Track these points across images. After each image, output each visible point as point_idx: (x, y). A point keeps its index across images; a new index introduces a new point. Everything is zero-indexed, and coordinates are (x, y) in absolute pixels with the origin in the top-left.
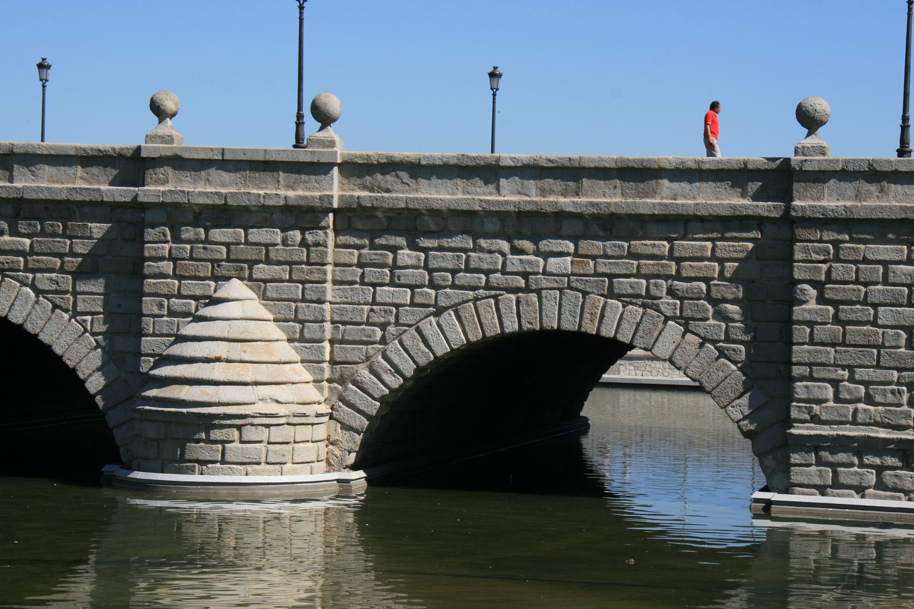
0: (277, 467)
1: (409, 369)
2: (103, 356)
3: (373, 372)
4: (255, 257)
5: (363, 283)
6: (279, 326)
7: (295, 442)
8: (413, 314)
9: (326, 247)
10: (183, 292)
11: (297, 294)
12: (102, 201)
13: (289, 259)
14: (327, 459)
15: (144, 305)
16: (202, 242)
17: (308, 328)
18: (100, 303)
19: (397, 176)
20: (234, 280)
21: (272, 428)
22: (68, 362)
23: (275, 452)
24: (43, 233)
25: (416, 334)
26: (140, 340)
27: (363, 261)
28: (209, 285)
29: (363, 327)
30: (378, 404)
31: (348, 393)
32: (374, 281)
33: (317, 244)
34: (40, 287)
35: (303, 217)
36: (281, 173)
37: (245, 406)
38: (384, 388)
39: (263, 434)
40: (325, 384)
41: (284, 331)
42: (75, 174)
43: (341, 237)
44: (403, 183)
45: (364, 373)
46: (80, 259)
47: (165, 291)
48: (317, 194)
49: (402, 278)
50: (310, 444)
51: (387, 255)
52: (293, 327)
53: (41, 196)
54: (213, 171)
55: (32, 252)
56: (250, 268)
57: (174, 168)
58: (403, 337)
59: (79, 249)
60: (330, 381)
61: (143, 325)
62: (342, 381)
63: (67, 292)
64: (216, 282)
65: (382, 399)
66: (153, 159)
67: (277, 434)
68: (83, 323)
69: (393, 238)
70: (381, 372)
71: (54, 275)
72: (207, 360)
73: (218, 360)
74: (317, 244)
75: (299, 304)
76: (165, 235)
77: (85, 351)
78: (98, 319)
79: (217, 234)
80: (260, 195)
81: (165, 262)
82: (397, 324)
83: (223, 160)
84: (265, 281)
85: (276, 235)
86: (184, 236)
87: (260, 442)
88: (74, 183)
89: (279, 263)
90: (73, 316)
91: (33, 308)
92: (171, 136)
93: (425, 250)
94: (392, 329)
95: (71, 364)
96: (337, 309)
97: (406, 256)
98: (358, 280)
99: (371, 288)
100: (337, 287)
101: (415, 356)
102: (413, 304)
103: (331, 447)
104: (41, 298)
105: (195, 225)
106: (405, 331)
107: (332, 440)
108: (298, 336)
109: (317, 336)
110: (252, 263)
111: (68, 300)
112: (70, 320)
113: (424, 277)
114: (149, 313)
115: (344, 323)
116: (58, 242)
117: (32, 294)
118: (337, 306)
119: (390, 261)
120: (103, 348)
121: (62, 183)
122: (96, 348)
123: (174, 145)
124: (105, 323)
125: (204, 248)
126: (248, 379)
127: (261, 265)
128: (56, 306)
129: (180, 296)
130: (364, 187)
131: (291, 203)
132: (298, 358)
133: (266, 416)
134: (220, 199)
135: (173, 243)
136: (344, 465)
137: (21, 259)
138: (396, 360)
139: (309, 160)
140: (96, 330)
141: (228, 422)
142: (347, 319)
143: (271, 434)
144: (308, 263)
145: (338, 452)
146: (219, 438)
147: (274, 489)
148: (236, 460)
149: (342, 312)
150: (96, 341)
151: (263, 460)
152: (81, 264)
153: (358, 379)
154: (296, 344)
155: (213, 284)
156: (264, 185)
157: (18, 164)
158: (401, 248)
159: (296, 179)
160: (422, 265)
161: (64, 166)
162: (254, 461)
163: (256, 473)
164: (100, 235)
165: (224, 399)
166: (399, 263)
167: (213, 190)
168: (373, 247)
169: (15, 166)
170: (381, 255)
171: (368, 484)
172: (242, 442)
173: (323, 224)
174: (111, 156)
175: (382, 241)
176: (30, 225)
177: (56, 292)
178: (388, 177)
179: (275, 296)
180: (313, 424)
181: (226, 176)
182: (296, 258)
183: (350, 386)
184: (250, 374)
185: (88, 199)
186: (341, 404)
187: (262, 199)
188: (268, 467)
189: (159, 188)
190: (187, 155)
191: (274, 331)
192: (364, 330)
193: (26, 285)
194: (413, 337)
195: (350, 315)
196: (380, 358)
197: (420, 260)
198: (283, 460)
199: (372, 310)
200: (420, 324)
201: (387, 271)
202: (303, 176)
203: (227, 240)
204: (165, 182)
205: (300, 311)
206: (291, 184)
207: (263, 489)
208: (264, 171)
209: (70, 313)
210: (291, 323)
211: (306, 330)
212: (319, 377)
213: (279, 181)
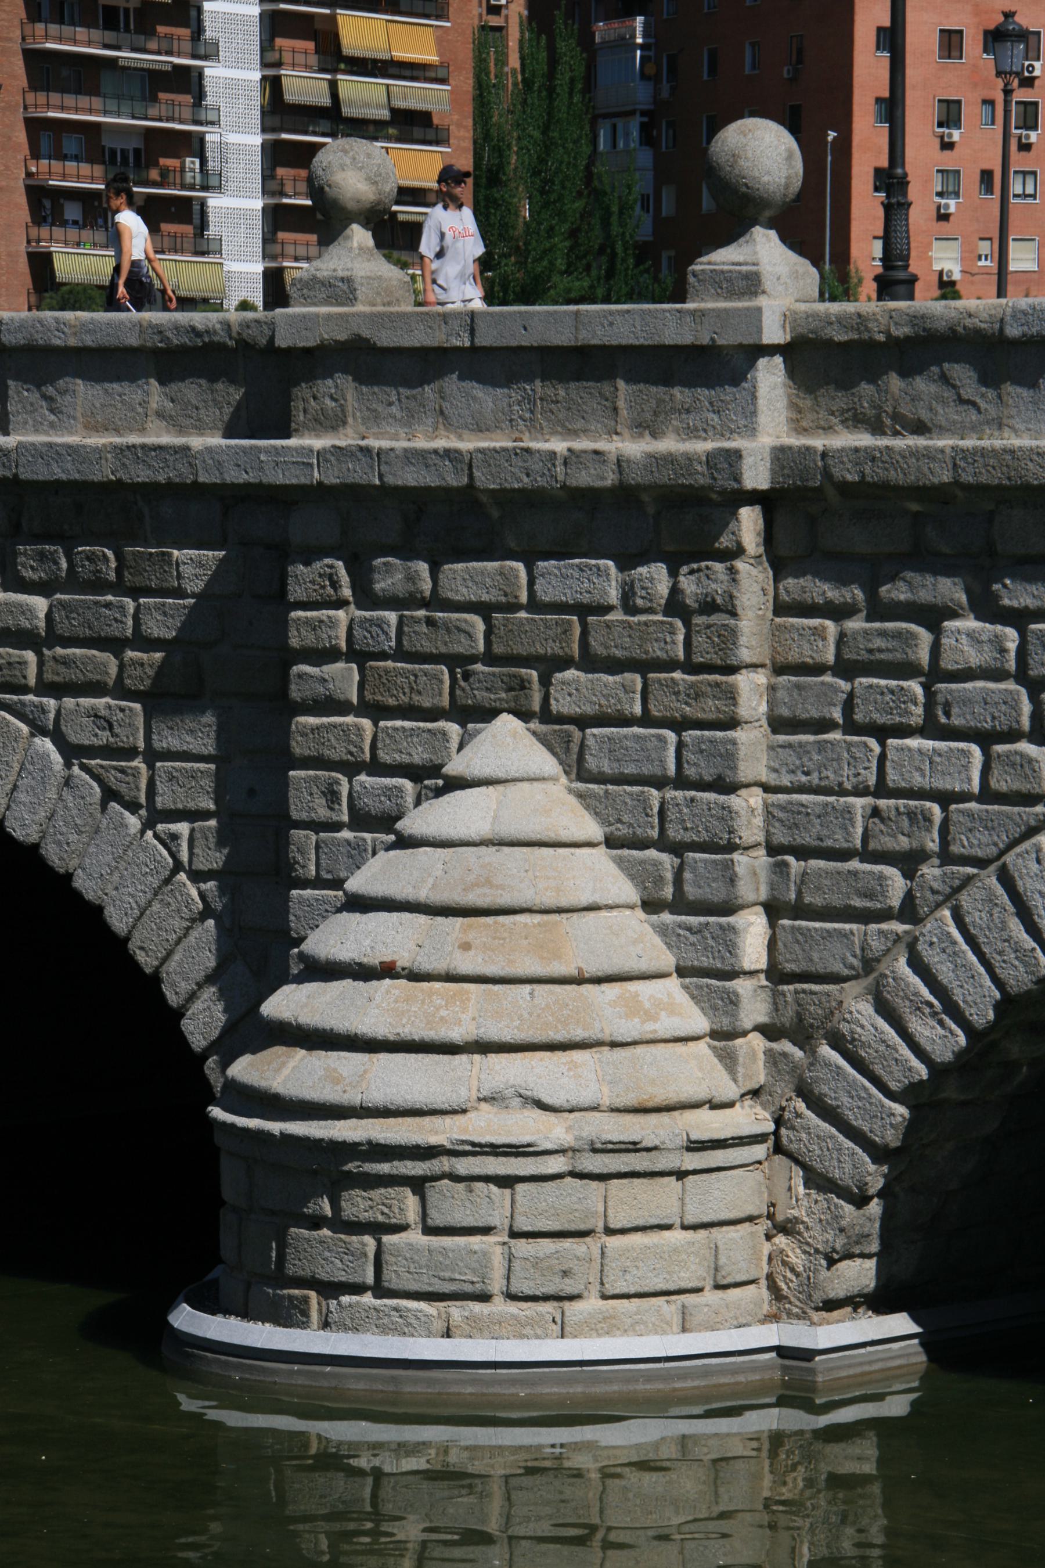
0: (547, 1308)
1: (980, 1002)
2: (219, 940)
3: (885, 1009)
4: (552, 648)
5: (851, 727)
6: (619, 862)
7: (610, 1231)
8: (987, 823)
9: (734, 614)
10: (384, 756)
11: (662, 762)
12: (195, 483)
13: (637, 653)
14: (770, 1277)
15: (292, 793)
16: (425, 604)
17: (694, 870)
18: (208, 784)
19: (945, 379)
20: (504, 716)
21: (520, 1188)
22: (141, 957)
23: (536, 1262)
24: (73, 582)
25: (1000, 890)
26: (287, 899)
27: (849, 655)
28: (444, 733)
29: (855, 864)
30: (901, 1110)
31: (821, 1073)
32: (881, 719)
33: (709, 607)
34: (73, 738)
35: (676, 518)
36: (621, 384)
37: (437, 1121)
38: (915, 1063)
39: (494, 1206)
40: (757, 1041)
41: (632, 877)
42: (144, 403)
43: (791, 581)
44: (961, 401)
45: (860, 1012)
46: (158, 655)
47: (338, 752)
48: (702, 447)
49: (955, 710)
50: (677, 1236)
51: (913, 636)
52: (656, 864)
53: (58, 473)
54: (452, 383)
55: (53, 637)
56: (545, 682)
57: (361, 379)
58: (965, 899)
59: (159, 628)
60: (769, 1032)
61: (293, 852)
62: (802, 1034)
63: (130, 753)
64: (463, 725)
65: (909, 1095)
66: (307, 351)
67: (537, 1206)
68: (170, 841)
69: (929, 579)
70: (904, 1009)
71: (101, 702)
72: (364, 973)
73: (388, 971)
74: (709, 607)
75: (671, 794)
76: (335, 585)
77: (179, 924)
78: (202, 830)
79: (469, 578)
80: (553, 454)
81: (340, 665)
82: (946, 857)
83: (474, 349)
84: (583, 722)
85: (607, 580)
86: (381, 585)
87: (486, 1230)
88: (143, 430)
89: (614, 666)
90: (148, 824)
91: (60, 798)
92: (348, 280)
93: (1019, 619)
94: (930, 871)
95: (146, 961)
96: (782, 808)
97: (967, 637)
98: (837, 715)
99: (873, 743)
100: (782, 738)
101: (996, 960)
102: (987, 795)
103: (781, 1240)
104: (76, 770)
105: (407, 553)
106: (968, 880)
107: (780, 1217)
108: (668, 892)
109: (715, 893)
110: (551, 666)
111: (136, 771)
112: (143, 832)
113: (1016, 707)
114: (304, 816)
115: (802, 853)
116: (108, 605)
117: (56, 758)
118: (782, 797)
119: (924, 656)
120: (218, 919)
121: (117, 431)
122: (203, 916)
123: (360, 308)
124: (220, 843)
125: (430, 622)
126: (456, 1034)
127: (571, 674)
128: (110, 795)
129: (377, 768)
130: (856, 420)
131: (635, 477)
132: (667, 960)
133: (495, 1150)
134: (456, 471)
135: (359, 607)
136: (818, 1297)
137: (30, 656)
138: (945, 972)
139: (687, 339)
140: (201, 865)
141: (385, 1168)
142: (806, 839)
143: (519, 1208)
144: (691, 667)
145: (797, 1258)
146: (365, 1216)
147: (513, 1382)
148: (413, 1287)
149: (796, 816)
150: (202, 895)
151: (496, 1285)
152: (162, 669)
153: (844, 1028)
154: (667, 917)
155: (453, 729)
156: (580, 424)
157: (17, 378)
158: (954, 615)
159: (660, 402)
160: (1012, 665)
161: (118, 379)
162: (468, 1288)
163: (476, 1328)
164: (201, 585)
165: (376, 1096)
166: (947, 663)
167: (440, 444)
168: (878, 610)
169: (10, 382)
170: (898, 635)
171: (931, 1359)
172: (430, 1230)
173: (725, 542)
174: (221, 347)
175: (896, 592)
176: (42, 557)
177: (108, 752)
178: (920, 384)
179: (607, 767)
180: (681, 1175)
181: (487, 398)
182: (657, 651)
183: (826, 1051)
184: (465, 1017)
185: (161, 478)
186: (801, 1105)
187: (560, 469)
188: (513, 1308)
189: (340, 438)
190: (385, 339)
191: (602, 876)
192: (854, 874)
193: (43, 732)
194: (991, 900)
195: (816, 828)
196: (902, 966)
197: (1003, 651)
198: (569, 1287)
199: (876, 812)
200: (1009, 858)
201: (915, 687)
202: (677, 392)
203: (485, 597)
204: (335, 422)
205: (672, 814)
206: (648, 416)
207: (473, 1381)
208: (578, 379)
209: (143, 812)
210: (652, 853)
211: (687, 875)
212: (725, 1023)
213: (615, 409)
